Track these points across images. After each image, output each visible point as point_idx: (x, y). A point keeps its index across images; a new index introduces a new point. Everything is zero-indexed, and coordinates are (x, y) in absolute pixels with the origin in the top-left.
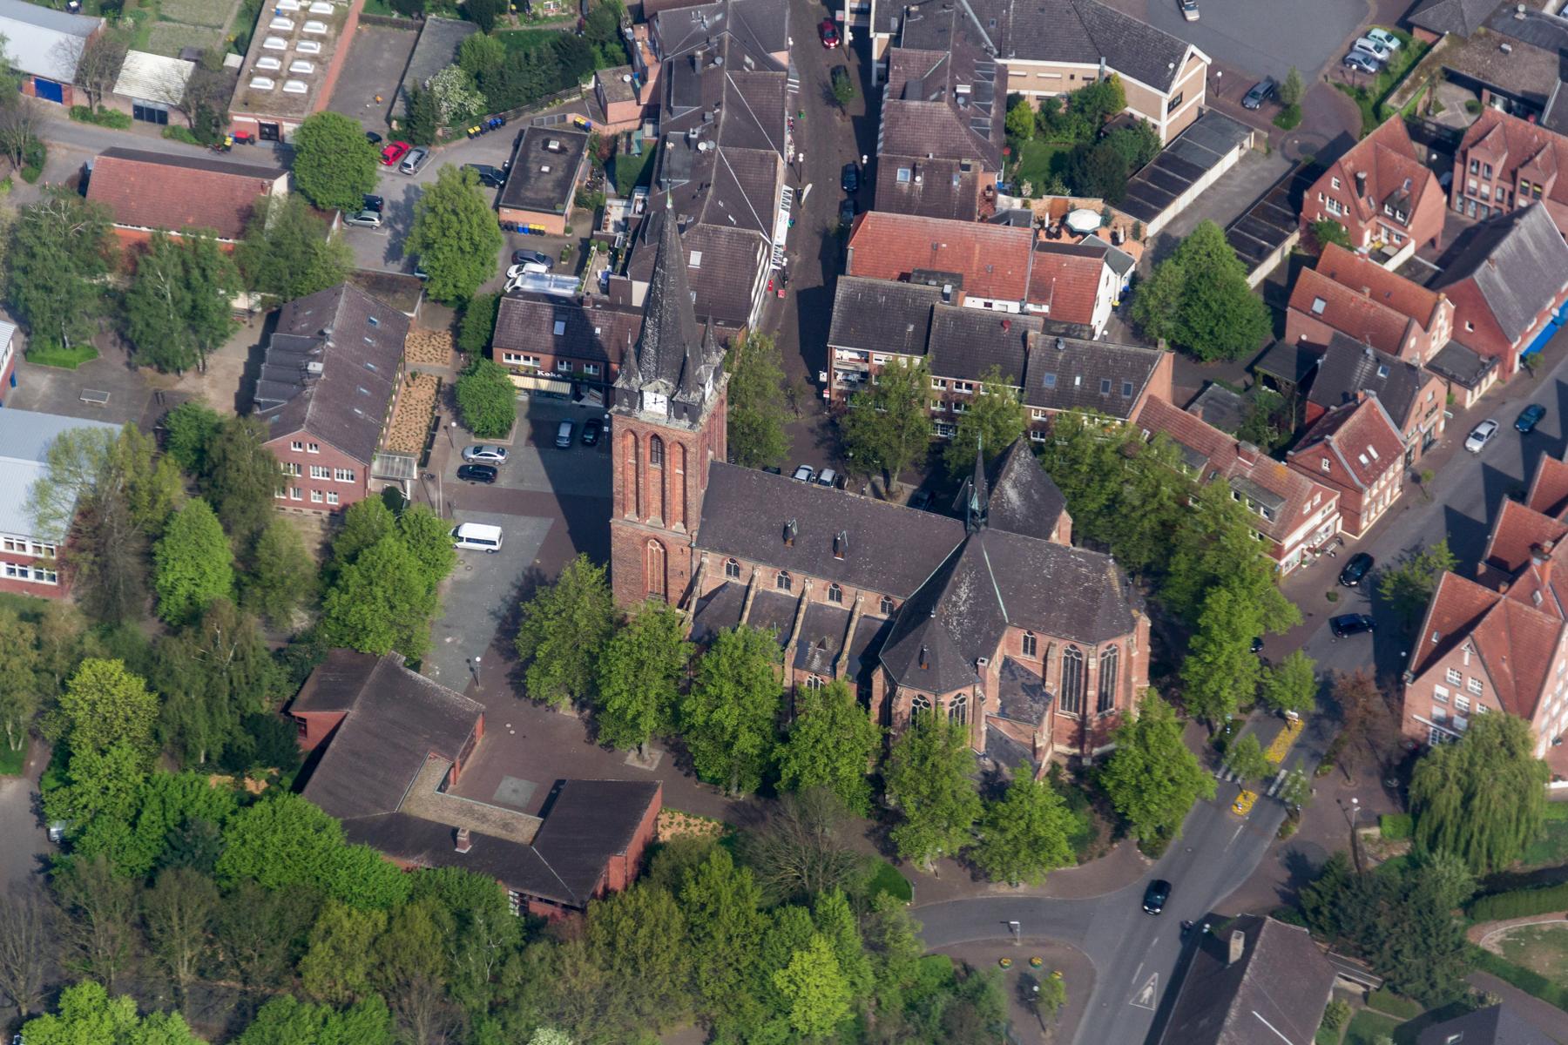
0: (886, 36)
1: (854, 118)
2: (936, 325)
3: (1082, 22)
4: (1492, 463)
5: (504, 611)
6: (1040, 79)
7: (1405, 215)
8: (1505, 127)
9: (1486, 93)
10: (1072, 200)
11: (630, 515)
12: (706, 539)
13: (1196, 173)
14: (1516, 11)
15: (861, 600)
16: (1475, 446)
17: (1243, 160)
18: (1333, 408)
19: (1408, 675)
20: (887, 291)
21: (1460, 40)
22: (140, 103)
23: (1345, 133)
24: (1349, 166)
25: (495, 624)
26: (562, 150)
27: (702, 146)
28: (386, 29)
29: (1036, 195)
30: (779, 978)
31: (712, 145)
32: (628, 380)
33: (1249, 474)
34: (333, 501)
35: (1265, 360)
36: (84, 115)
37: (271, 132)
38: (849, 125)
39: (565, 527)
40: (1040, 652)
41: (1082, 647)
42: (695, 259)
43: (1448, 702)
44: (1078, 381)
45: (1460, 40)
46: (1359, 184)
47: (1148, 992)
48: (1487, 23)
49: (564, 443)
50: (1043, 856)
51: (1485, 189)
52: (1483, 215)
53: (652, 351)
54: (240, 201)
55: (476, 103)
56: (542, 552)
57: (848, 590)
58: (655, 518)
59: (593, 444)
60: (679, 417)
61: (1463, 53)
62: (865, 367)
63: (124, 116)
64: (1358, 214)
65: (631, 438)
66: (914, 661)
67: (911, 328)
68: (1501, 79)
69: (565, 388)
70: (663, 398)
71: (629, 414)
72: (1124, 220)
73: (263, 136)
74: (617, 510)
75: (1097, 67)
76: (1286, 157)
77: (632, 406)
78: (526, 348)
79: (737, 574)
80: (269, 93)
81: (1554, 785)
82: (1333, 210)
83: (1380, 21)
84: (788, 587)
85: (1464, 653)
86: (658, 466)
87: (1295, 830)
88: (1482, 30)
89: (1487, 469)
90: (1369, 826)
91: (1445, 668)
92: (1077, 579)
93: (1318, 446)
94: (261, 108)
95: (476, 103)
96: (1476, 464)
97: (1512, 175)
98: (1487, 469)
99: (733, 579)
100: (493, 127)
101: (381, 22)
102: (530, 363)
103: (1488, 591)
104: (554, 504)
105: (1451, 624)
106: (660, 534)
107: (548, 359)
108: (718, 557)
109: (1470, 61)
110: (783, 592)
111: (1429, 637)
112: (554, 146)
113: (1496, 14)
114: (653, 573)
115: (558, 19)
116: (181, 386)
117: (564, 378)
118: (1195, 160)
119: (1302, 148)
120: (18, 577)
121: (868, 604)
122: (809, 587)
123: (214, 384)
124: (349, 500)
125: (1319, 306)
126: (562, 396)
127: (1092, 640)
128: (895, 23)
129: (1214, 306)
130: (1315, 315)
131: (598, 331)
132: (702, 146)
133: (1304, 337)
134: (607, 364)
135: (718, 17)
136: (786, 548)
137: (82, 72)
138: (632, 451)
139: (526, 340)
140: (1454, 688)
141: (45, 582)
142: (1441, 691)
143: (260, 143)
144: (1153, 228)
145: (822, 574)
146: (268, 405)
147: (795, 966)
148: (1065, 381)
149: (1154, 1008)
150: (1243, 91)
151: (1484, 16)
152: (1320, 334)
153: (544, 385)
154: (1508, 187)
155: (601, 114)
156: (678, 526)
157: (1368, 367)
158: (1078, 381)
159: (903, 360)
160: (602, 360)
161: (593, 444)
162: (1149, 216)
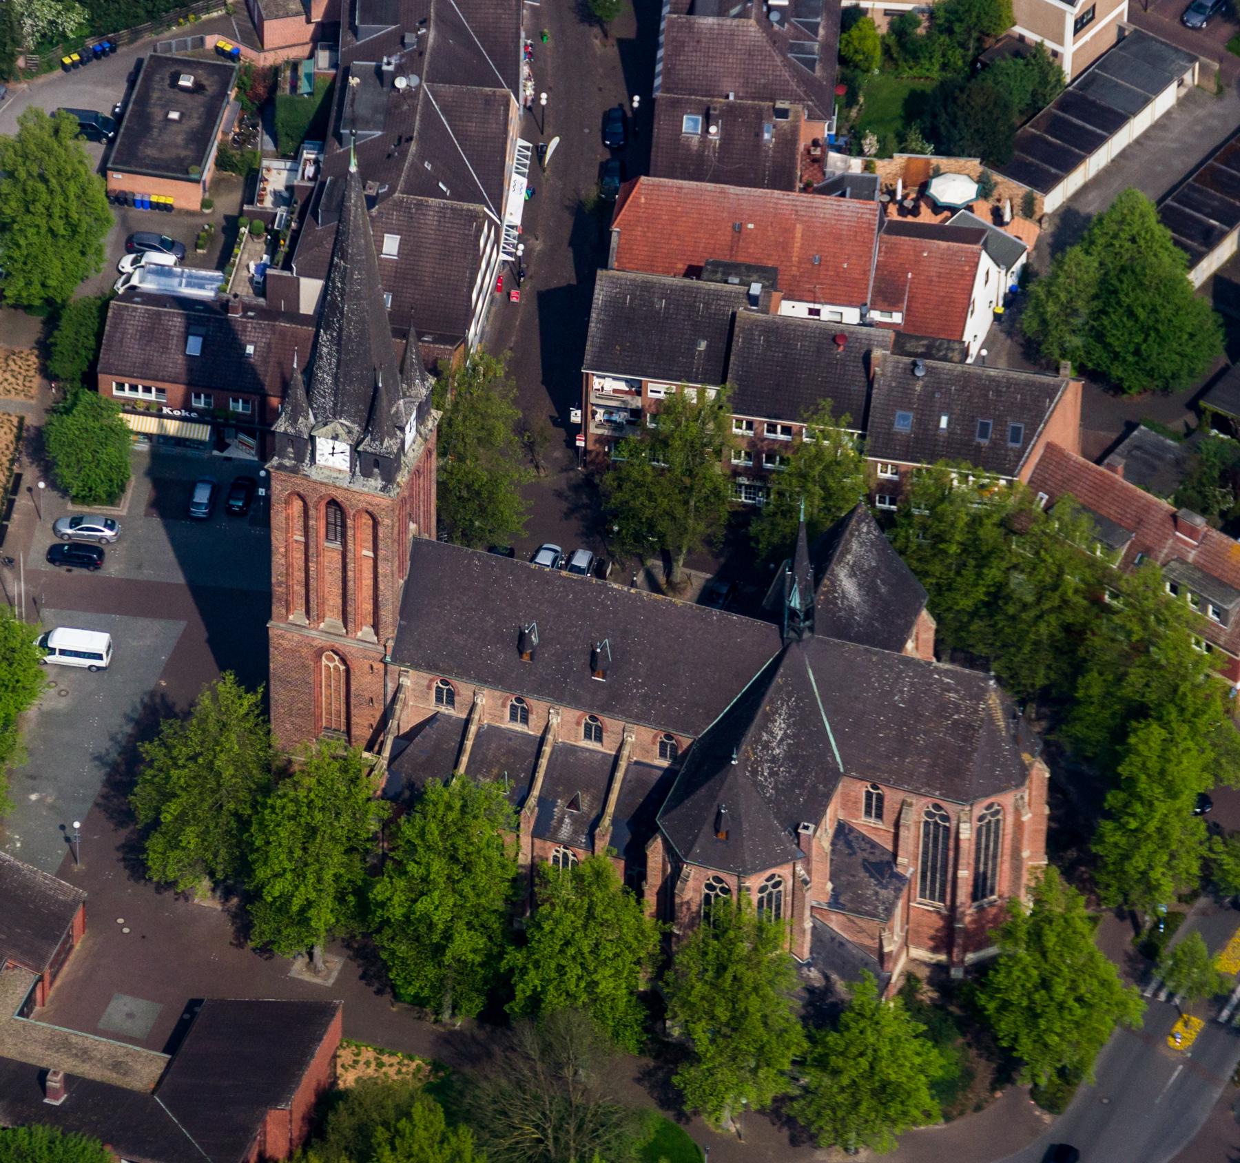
1: (622, 43)
2: (738, 341)
10: (936, 160)
11: (298, 616)
12: (408, 650)
13: (1116, 121)
15: (631, 739)
20: (667, 292)
26: (198, 88)
27: (401, 83)
31: (415, 80)
32: (294, 420)
33: (1192, 556)
40: (889, 815)
41: (950, 808)
53: (329, 379)
56: (169, 671)
58: (332, 620)
60: (367, 474)
62: (637, 402)
65: (297, 505)
66: (707, 828)
67: (703, 346)
69: (202, 432)
70: (343, 446)
71: (294, 470)
72: (1010, 189)
74: (277, 609)
77: (299, 458)
78: (146, 374)
86: (337, 545)
92: (942, 709)
99: (444, 709)
100: (98, 55)
102: (152, 397)
104: (187, 601)
112: (186, 82)
118: (1113, 102)
121: (639, 745)
122: (555, 721)
127: (966, 797)
129: (1142, 314)
131: (250, 349)
132: (401, 83)
134: (264, 397)
136: (522, 664)
139: (146, 364)
144: (1052, 201)
145: (574, 701)
153: (172, 427)
156: (366, 632)
162: (1046, 183)
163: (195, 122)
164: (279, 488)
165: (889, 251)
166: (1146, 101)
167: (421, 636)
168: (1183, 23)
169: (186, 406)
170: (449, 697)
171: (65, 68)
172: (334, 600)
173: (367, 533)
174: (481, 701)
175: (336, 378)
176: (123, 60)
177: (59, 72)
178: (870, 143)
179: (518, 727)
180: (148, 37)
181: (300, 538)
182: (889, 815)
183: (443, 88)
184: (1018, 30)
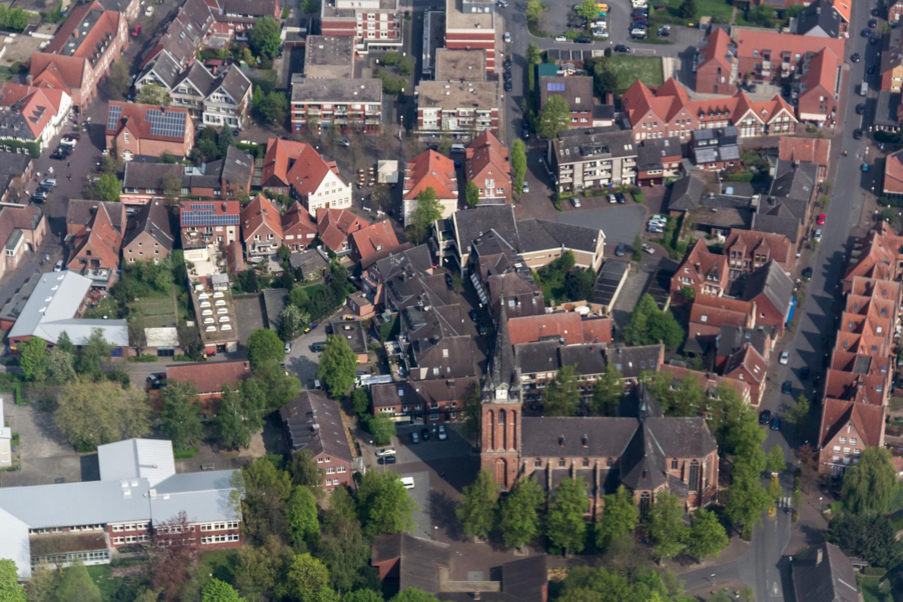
0: (467, 255)
1: (462, 293)
2: (563, 355)
3: (547, 231)
5: (429, 510)
6: (537, 259)
7: (717, 277)
8: (742, 236)
9: (713, 230)
11: (490, 450)
12: (526, 452)
13: (617, 283)
14: (709, 196)
15: (598, 462)
16: (784, 361)
17: (629, 275)
18: (731, 355)
19: (819, 446)
20: (536, 347)
21: (694, 211)
22: (160, 348)
24: (692, 262)
25: (428, 516)
26: (352, 329)
27: (426, 309)
28: (244, 300)
29: (558, 304)
32: (489, 386)
36: (137, 359)
37: (222, 349)
38: (461, 296)
39: (435, 474)
40: (680, 466)
41: (698, 460)
43: (841, 451)
44: (631, 364)
46: (697, 268)
47: (776, 590)
48: (700, 203)
49: (416, 441)
51: (739, 263)
52: (738, 275)
53: (498, 372)
55: (306, 318)
56: (431, 484)
57: (592, 460)
58: (500, 449)
61: (698, 216)
62: (534, 381)
63: (154, 356)
64: (698, 282)
65: (490, 414)
67: (551, 359)
69: (408, 418)
70: (505, 391)
71: (490, 402)
72: (598, 307)
73: (219, 351)
74: (483, 449)
75: (560, 249)
76: (645, 271)
77: (491, 398)
78: (388, 404)
80: (215, 332)
82: (686, 283)
83: (654, 212)
85: (848, 428)
86: (502, 424)
88: (700, 206)
90: (826, 509)
91: (839, 438)
95: (306, 318)
97: (751, 254)
98: (794, 370)
99: (539, 468)
100: (313, 328)
101: (242, 297)
103: (847, 402)
104: (426, 466)
105: (833, 420)
106: (504, 455)
107: (399, 407)
110: (562, 468)
111: (824, 428)
113: (701, 199)
114: (500, 474)
115: (315, 281)
116: (241, 455)
117: (407, 414)
118: (615, 279)
119: (649, 267)
120: (220, 542)
121: (602, 464)
122: (574, 462)
126: (406, 422)
127: (702, 455)
128: (469, 249)
129: (663, 326)
130: (703, 323)
131: (417, 390)
132: (426, 309)
133: (699, 334)
134: (426, 403)
135: (402, 259)
136: (561, 447)
138: (490, 420)
141: (233, 540)
143: (218, 354)
144: (610, 308)
145: (579, 455)
148: (625, 366)
149: (781, 595)
150: (613, 250)
151: (698, 200)
152: (708, 331)
153: (399, 419)
154: (749, 260)
155: (357, 312)
156: (512, 450)
157: (741, 335)
158: (631, 364)
161: (428, 439)
162: (608, 303)
164: (485, 409)
166: (621, 276)
167: (531, 446)
168: (616, 255)
169: (402, 411)
170: (539, 463)
171: (305, 333)
172: (501, 442)
173: (512, 418)
174: (551, 462)
175: (501, 371)
176: (322, 327)
177: (304, 335)
178: (553, 302)
179: (562, 468)
180: (325, 320)
181: (490, 424)
182: (680, 466)
183: (439, 307)
184: (576, 265)
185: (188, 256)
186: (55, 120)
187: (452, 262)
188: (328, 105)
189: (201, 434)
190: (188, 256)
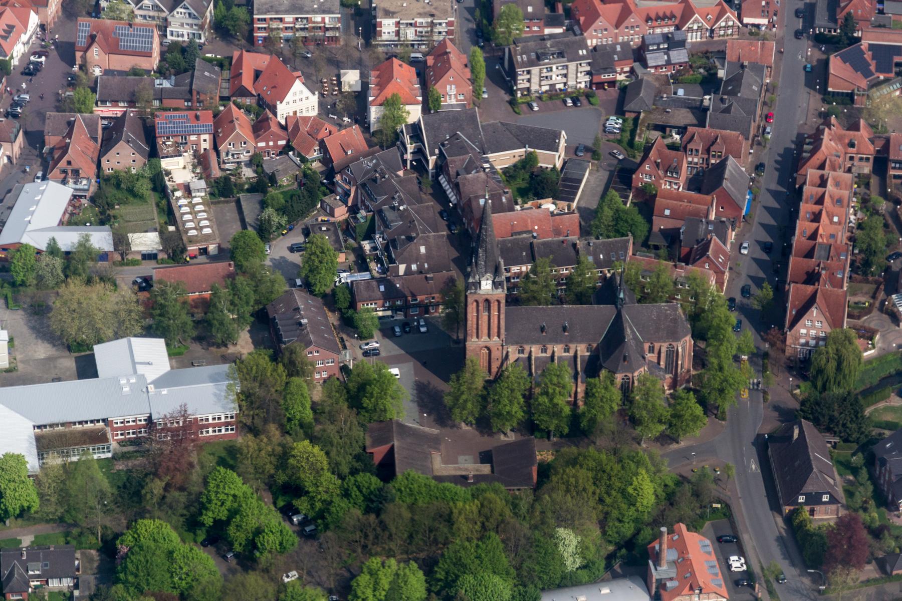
2: (536, 249)
4: (754, 256)
7: (677, 173)
9: (668, 129)
10: (540, 201)
11: (475, 339)
12: (509, 341)
13: (580, 181)
14: (662, 97)
15: (579, 349)
16: (745, 252)
19: (786, 329)
20: (510, 241)
21: (649, 112)
22: (144, 252)
23: (95, 375)
25: (415, 405)
26: (328, 230)
27: (401, 208)
28: (221, 205)
30: (630, 490)
31: (405, 206)
33: (683, 275)
34: (325, 375)
35: (651, 238)
37: (204, 251)
40: (656, 351)
41: (674, 344)
42: (423, 249)
43: (807, 334)
44: (601, 256)
45: (649, 112)
49: (398, 334)
50: (699, 423)
51: (696, 160)
54: (222, 273)
55: (284, 220)
56: (416, 374)
57: (573, 346)
58: (485, 338)
59: (410, 332)
60: (497, 288)
61: (652, 116)
65: (475, 304)
66: (622, 361)
68: (673, 122)
69: (389, 313)
70: (490, 282)
71: (475, 293)
72: (563, 204)
73: (201, 254)
77: (476, 289)
78: (371, 299)
79: (523, 353)
81: (865, 354)
84: (546, 352)
87: (770, 398)
89: (755, 260)
91: (805, 321)
92: (666, 316)
93: (703, 259)
94: (197, 242)
95: (284, 220)
96: (748, 258)
97: (708, 151)
100: (290, 230)
102: (373, 306)
104: (408, 357)
105: (799, 304)
107: (380, 302)
108: (515, 347)
109: (658, 119)
110: (544, 355)
111: (791, 312)
112: (324, 229)
115: (288, 185)
116: (229, 351)
122: (556, 349)
123: (242, 347)
124: (332, 373)
125: (667, 212)
126: (388, 316)
130: (667, 217)
132: (401, 208)
134: (406, 297)
136: (543, 334)
137: (116, 245)
138: (475, 310)
139: (370, 297)
140: (808, 329)
141: (230, 432)
142: (803, 331)
143: (200, 257)
144: (574, 205)
145: (560, 342)
146: (289, 341)
147: (635, 483)
153: (380, 314)
154: (706, 156)
156: (496, 338)
158: (601, 256)
159: (524, 269)
160: (403, 297)
161: (410, 332)
162: (573, 200)
163: (333, 238)
165: (554, 221)
169: (383, 306)
171: (283, 235)
172: (485, 331)
175: (485, 262)
182: (656, 351)
184: (540, 165)
185: (165, 164)
186: (24, 38)
187: (420, 166)
188: (289, 18)
189: (193, 333)
190: (165, 164)
